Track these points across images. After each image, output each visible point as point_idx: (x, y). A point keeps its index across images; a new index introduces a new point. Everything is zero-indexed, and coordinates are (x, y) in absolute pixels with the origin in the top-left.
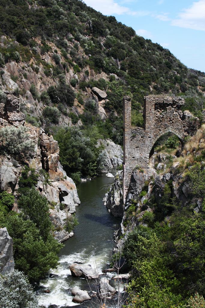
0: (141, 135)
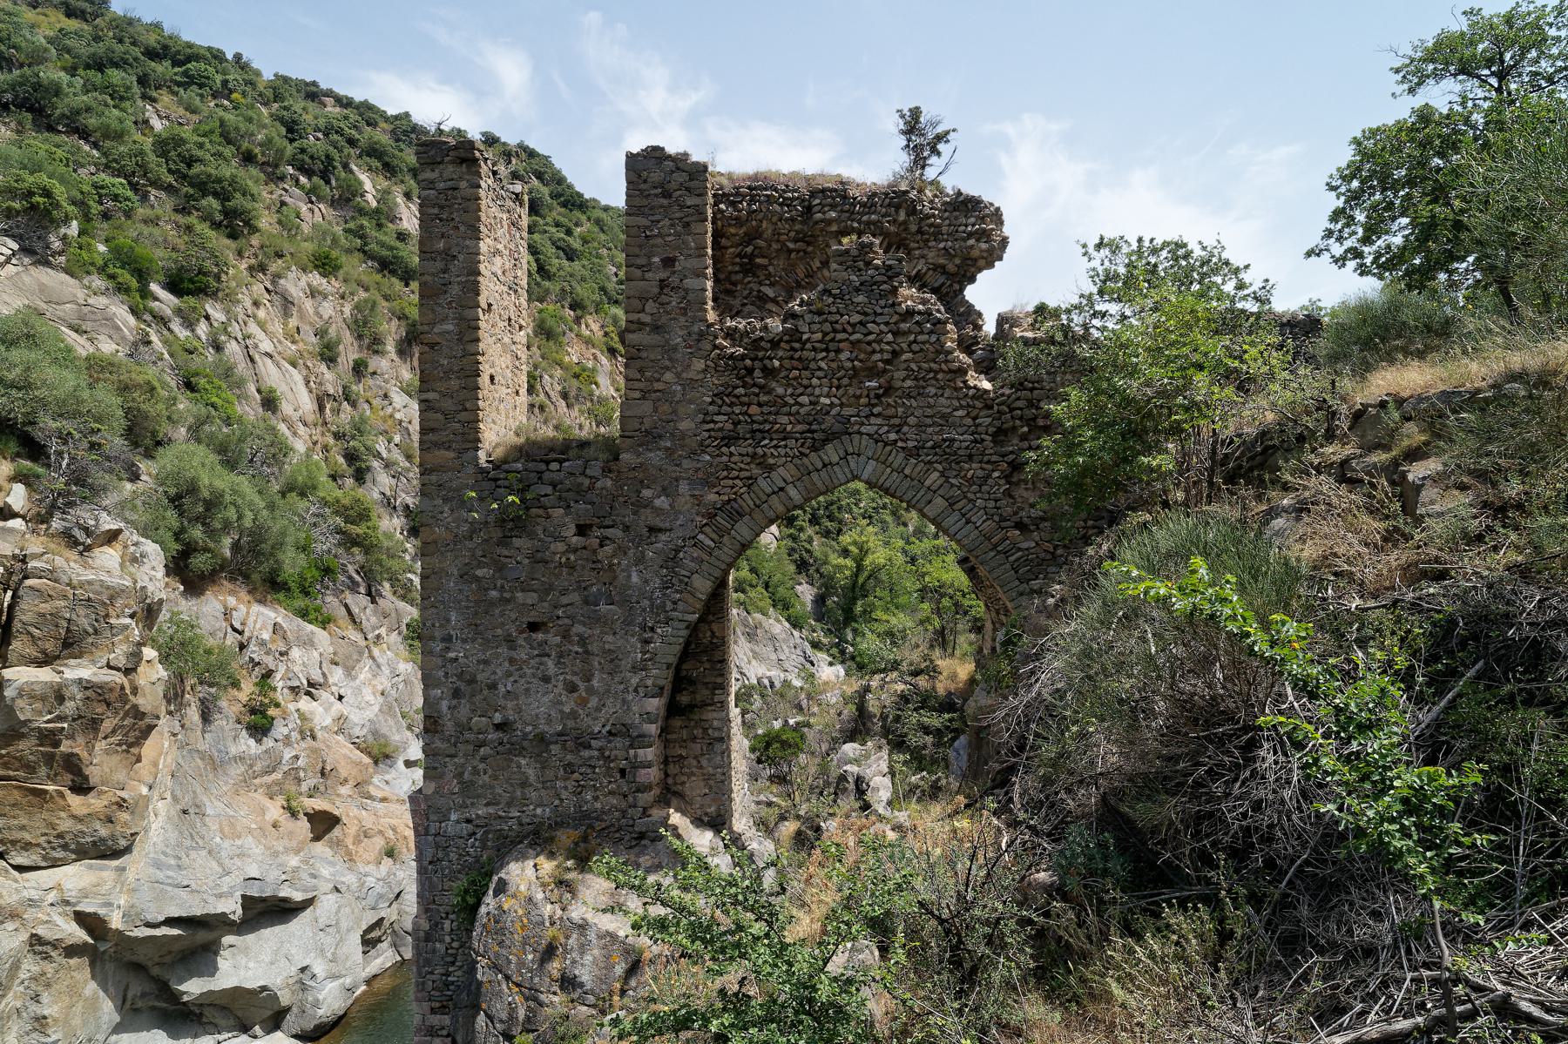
0: (582, 506)
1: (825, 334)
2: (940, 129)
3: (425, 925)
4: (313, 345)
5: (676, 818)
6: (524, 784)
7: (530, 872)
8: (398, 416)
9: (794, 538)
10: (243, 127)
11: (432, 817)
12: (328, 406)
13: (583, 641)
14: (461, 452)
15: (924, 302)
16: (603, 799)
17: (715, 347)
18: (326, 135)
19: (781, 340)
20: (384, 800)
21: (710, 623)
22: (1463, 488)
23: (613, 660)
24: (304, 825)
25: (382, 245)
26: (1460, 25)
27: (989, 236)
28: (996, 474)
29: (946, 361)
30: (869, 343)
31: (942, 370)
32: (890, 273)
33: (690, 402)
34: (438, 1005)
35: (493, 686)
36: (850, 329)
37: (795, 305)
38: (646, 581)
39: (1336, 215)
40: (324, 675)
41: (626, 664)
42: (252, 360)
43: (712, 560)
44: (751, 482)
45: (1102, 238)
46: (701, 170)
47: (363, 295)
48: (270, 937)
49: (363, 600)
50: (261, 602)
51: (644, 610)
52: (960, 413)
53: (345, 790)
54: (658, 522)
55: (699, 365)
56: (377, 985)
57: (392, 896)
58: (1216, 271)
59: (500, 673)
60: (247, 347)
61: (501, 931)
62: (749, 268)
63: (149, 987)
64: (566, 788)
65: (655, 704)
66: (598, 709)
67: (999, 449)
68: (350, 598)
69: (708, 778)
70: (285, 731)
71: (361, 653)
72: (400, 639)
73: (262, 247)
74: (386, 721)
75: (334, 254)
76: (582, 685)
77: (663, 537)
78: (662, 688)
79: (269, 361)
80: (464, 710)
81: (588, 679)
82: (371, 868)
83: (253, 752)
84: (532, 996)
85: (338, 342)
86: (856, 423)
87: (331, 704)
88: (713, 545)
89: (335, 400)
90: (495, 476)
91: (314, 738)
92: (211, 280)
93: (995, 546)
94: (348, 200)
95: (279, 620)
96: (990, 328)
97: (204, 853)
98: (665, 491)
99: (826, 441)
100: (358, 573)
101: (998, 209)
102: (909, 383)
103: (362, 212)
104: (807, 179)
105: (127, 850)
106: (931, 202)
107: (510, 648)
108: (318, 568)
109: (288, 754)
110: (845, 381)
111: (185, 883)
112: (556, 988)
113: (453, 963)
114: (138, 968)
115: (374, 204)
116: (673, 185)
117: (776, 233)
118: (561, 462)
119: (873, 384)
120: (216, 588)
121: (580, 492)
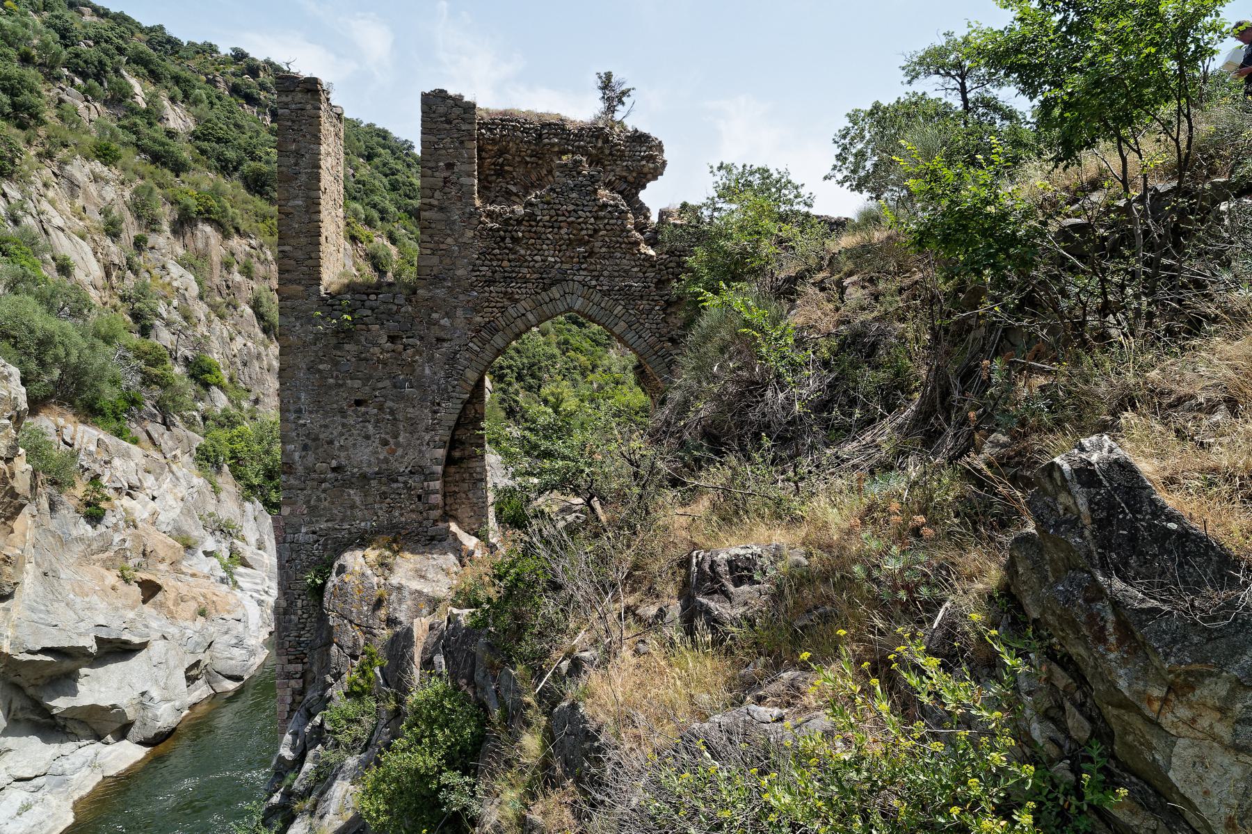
0: (391, 323)
1: (552, 217)
2: (624, 88)
3: (284, 604)
4: (99, 222)
5: (454, 527)
6: (353, 507)
7: (361, 560)
8: (175, 284)
9: (504, 391)
10: (20, 31)
11: (288, 531)
12: (114, 274)
13: (392, 412)
14: (307, 287)
15: (614, 199)
16: (406, 516)
17: (481, 223)
18: (97, 43)
19: (523, 220)
20: (193, 575)
21: (474, 405)
22: (864, 287)
23: (413, 424)
24: (136, 591)
25: (155, 140)
26: (941, 42)
27: (655, 159)
28: (657, 308)
29: (627, 237)
30: (579, 224)
31: (624, 242)
32: (593, 180)
33: (464, 257)
34: (293, 657)
35: (331, 442)
36: (567, 214)
37: (532, 198)
38: (435, 373)
39: (838, 157)
40: (140, 480)
41: (422, 426)
42: (46, 232)
43: (479, 360)
44: (503, 310)
45: (722, 164)
46: (471, 107)
47: (140, 182)
48: (115, 671)
49: (162, 428)
50: (84, 423)
51: (433, 392)
52: (635, 269)
53: (163, 567)
54: (443, 335)
55: (470, 234)
56: (199, 709)
57: (206, 645)
58: (785, 187)
59: (335, 434)
60: (41, 221)
61: (345, 595)
62: (500, 173)
63: (27, 703)
64: (381, 508)
65: (441, 453)
66: (403, 457)
67: (659, 292)
68: (150, 427)
69: (473, 505)
70: (114, 520)
71: (162, 469)
72: (191, 460)
73: (48, 137)
74: (186, 521)
75: (114, 146)
76: (392, 441)
77: (445, 345)
78: (445, 442)
79: (61, 234)
80: (311, 458)
81: (396, 437)
82: (189, 623)
83: (90, 535)
84: (368, 631)
85: (122, 221)
86: (571, 274)
87: (147, 503)
88: (478, 349)
89: (120, 269)
90: (332, 302)
91: (136, 527)
92: (7, 163)
93: (656, 352)
94: (120, 101)
95: (101, 436)
96: (654, 218)
97: (63, 604)
98: (447, 315)
99: (552, 284)
100: (155, 407)
101: (660, 142)
102: (604, 250)
103: (133, 111)
104: (539, 116)
105: (9, 596)
106: (618, 135)
107: (343, 417)
108: (125, 399)
109: (117, 538)
110: (564, 247)
111: (54, 623)
112: (383, 626)
113: (303, 629)
114: (18, 688)
115: (144, 106)
116: (453, 116)
117: (518, 150)
118: (377, 294)
119: (582, 249)
120: (47, 411)
121: (390, 314)
